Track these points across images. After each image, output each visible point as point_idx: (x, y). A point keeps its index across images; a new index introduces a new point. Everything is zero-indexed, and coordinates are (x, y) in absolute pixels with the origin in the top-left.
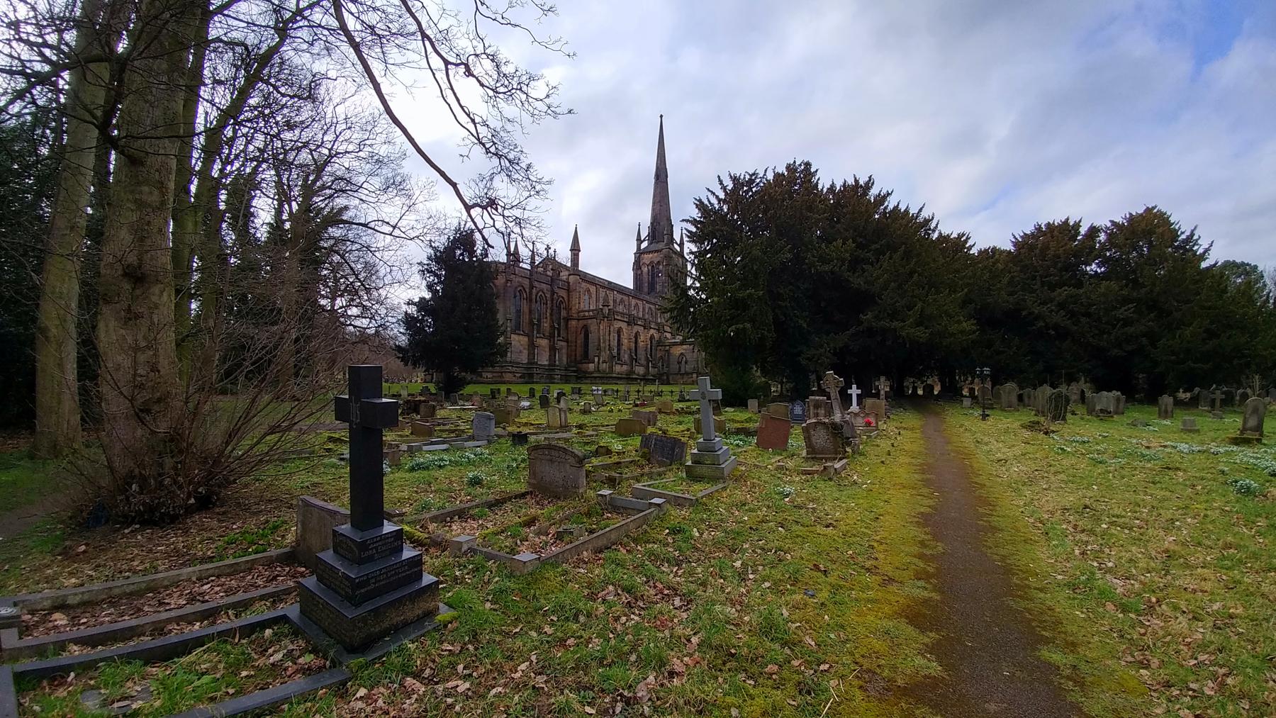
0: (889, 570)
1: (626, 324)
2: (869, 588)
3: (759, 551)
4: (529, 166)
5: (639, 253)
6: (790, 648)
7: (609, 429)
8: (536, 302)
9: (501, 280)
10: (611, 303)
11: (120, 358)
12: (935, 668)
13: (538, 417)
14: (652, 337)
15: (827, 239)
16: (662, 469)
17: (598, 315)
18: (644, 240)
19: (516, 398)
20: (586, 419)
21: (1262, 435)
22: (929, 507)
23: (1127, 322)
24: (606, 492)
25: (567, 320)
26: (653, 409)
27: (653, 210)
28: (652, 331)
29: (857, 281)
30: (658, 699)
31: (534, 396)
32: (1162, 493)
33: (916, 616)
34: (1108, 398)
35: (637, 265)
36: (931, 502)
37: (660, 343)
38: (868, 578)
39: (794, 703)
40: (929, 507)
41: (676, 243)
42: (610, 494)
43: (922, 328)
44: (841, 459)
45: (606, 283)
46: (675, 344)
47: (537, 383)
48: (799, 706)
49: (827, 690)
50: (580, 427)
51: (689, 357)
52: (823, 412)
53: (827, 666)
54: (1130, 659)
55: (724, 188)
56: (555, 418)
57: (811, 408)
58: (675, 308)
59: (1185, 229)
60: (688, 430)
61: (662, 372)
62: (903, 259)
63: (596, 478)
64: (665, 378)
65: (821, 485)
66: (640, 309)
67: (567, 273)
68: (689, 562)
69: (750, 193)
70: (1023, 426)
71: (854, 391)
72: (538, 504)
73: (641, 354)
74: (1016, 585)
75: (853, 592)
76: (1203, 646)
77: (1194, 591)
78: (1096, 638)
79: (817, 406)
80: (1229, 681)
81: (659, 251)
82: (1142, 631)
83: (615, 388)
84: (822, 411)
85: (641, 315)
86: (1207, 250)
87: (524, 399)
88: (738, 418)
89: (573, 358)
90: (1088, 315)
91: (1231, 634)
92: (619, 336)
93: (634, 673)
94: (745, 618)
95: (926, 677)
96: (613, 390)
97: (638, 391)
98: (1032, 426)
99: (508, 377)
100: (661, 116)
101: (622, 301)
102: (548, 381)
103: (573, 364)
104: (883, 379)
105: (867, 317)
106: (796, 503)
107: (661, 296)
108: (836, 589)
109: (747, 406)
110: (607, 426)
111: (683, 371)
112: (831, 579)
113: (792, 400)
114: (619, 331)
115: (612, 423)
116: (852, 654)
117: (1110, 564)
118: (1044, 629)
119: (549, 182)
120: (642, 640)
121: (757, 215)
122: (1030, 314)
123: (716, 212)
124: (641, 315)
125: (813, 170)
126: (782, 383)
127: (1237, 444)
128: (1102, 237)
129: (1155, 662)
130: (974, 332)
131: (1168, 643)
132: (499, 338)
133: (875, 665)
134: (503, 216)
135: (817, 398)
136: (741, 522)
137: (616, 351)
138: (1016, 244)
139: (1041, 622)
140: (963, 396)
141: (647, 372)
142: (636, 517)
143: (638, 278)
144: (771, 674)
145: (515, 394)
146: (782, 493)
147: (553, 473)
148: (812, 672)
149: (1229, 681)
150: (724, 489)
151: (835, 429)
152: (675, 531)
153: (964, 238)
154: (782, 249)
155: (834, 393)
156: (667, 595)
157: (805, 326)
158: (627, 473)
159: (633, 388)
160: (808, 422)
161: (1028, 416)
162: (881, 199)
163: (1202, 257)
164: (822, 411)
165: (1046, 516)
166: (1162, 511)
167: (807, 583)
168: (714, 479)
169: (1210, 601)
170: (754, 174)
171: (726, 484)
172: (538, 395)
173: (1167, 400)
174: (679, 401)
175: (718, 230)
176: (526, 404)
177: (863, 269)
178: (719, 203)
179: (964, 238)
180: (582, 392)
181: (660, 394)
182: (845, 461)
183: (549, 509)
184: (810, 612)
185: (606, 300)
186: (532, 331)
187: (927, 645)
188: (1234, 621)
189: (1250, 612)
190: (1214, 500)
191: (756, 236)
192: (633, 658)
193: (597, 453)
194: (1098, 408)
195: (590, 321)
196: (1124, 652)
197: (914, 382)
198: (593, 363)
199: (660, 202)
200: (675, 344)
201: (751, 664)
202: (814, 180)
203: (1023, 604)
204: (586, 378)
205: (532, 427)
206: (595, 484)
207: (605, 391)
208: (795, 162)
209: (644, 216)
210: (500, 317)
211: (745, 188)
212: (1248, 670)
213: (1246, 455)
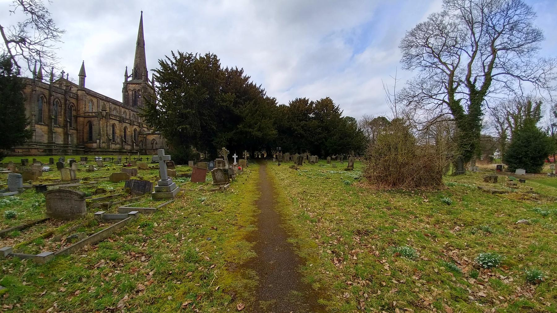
0: (241, 223)
1: (129, 125)
2: (233, 231)
3: (188, 227)
4: (50, 21)
5: (126, 84)
6: (198, 263)
7: (106, 179)
8: (54, 105)
9: (28, 90)
10: (108, 109)
12: (254, 254)
13: (56, 175)
14: (135, 130)
15: (225, 91)
16: (138, 197)
17: (99, 115)
19: (40, 165)
20: (90, 175)
21: (353, 168)
22: (258, 198)
23: (320, 133)
24: (101, 212)
25: (76, 117)
26: (136, 167)
27: (135, 61)
28: (135, 127)
29: (237, 111)
30: (130, 305)
31: (53, 163)
32: (325, 185)
33: (249, 238)
34: (314, 158)
35: (125, 90)
36: (259, 196)
37: (140, 133)
38: (234, 228)
39: (199, 285)
40: (258, 198)
41: (150, 81)
42: (103, 213)
43: (260, 132)
44: (227, 184)
46: (149, 134)
47: (55, 155)
48: (200, 285)
49: (213, 275)
50: (86, 179)
51: (158, 140)
52: (222, 165)
53: (214, 265)
54: (313, 237)
55: (175, 58)
56: (66, 174)
57: (217, 163)
58: (148, 115)
59: (336, 105)
60: (156, 177)
61: (142, 148)
62: (253, 104)
63: (94, 206)
65: (219, 195)
66: (128, 114)
67: (76, 89)
68: (151, 239)
69: (189, 63)
70: (290, 167)
71: (235, 156)
72: (54, 225)
74: (282, 220)
75: (227, 234)
76: (333, 230)
77: (331, 214)
78: (304, 232)
79: (219, 163)
80: (341, 239)
81: (140, 84)
82: (317, 227)
83: (111, 157)
84: (221, 165)
85: (128, 117)
86: (341, 113)
87: (45, 165)
88: (183, 170)
90: (309, 131)
91: (341, 225)
92: (113, 128)
93: (116, 297)
94: (178, 257)
95: (250, 259)
96: (110, 158)
97: (127, 159)
98: (292, 167)
99: (34, 152)
100: (142, 12)
101: (115, 109)
102: (63, 154)
103: (81, 144)
104: (246, 151)
105: (240, 126)
106: (207, 204)
107: (140, 109)
108: (220, 234)
109: (188, 164)
110: (104, 178)
112: (219, 231)
113: (209, 161)
114: (113, 126)
115: (108, 176)
116: (224, 258)
117: (309, 209)
118: (289, 232)
119: (62, 32)
120: (121, 281)
121: (192, 75)
122: (294, 129)
123: (170, 69)
124: (128, 117)
125: (218, 59)
126: (205, 153)
127: (346, 171)
128: (314, 105)
129: (320, 236)
130: (277, 134)
131: (323, 230)
132: (26, 127)
133: (233, 260)
134: (29, 48)
135: (219, 159)
136: (180, 216)
137: (111, 136)
138: (290, 104)
139: (288, 230)
140: (273, 158)
142: (119, 223)
143: (125, 97)
144: (189, 276)
145: (39, 162)
146: (201, 200)
147: (62, 206)
148: (207, 270)
149: (341, 239)
150: (173, 202)
151: (225, 172)
152: (143, 226)
153: (274, 100)
154: (204, 93)
155: (226, 157)
156: (138, 257)
157: (215, 128)
158: (116, 201)
159: (123, 157)
160: (214, 169)
161: (292, 164)
162: (246, 79)
163: (340, 115)
164: (221, 165)
165: (293, 196)
166: (324, 191)
167: (208, 235)
168: (167, 198)
169: (335, 216)
170: (191, 54)
171: (174, 200)
172: (55, 162)
173: (329, 158)
174: (152, 163)
175: (172, 78)
176: (47, 168)
177: (239, 106)
178: (172, 64)
179: (274, 100)
180: (88, 160)
181: (140, 160)
182: (229, 184)
183: (62, 226)
184: (208, 246)
185: (104, 107)
186: (51, 122)
187: (252, 247)
188: (342, 221)
189: (347, 218)
190: (338, 187)
191: (192, 84)
192: (116, 290)
193: (96, 193)
194: (311, 161)
195: (93, 119)
196: (311, 235)
197: (258, 153)
198: (96, 143)
199: (140, 57)
200: (149, 134)
201: (180, 276)
202: (218, 63)
203: (284, 225)
204: (91, 152)
205: (50, 181)
206: (94, 210)
207: (104, 159)
208: (209, 53)
209: (130, 63)
210: (27, 114)
211: (186, 60)
212: (347, 236)
213: (348, 173)
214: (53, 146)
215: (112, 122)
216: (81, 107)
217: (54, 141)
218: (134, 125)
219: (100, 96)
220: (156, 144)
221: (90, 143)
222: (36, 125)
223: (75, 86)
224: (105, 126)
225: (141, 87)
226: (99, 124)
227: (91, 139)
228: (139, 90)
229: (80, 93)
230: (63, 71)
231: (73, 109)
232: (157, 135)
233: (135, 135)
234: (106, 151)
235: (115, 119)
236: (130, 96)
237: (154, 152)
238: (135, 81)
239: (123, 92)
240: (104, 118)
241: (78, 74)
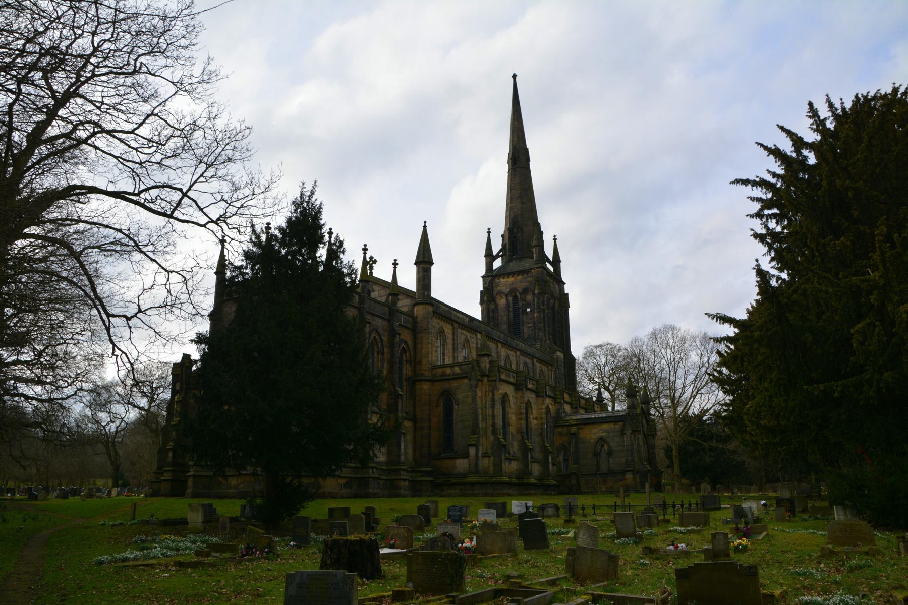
5: (490, 277)
11: (666, 401)
18: (498, 256)
25: (413, 382)
45: (467, 319)
64: (574, 482)
73: (534, 442)
100: (514, 76)
111: (604, 468)
141: (525, 472)
195: (455, 384)
198: (466, 456)
216: (424, 351)
219: (458, 317)
220: (610, 453)
221: (449, 458)
223: (406, 293)
224: (489, 405)
226: (474, 398)
227: (449, 447)
228: (525, 291)
231: (404, 359)
232: (612, 425)
234: (493, 484)
235: (507, 379)
238: (514, 266)
239: (482, 302)
240: (486, 379)
241: (414, 262)
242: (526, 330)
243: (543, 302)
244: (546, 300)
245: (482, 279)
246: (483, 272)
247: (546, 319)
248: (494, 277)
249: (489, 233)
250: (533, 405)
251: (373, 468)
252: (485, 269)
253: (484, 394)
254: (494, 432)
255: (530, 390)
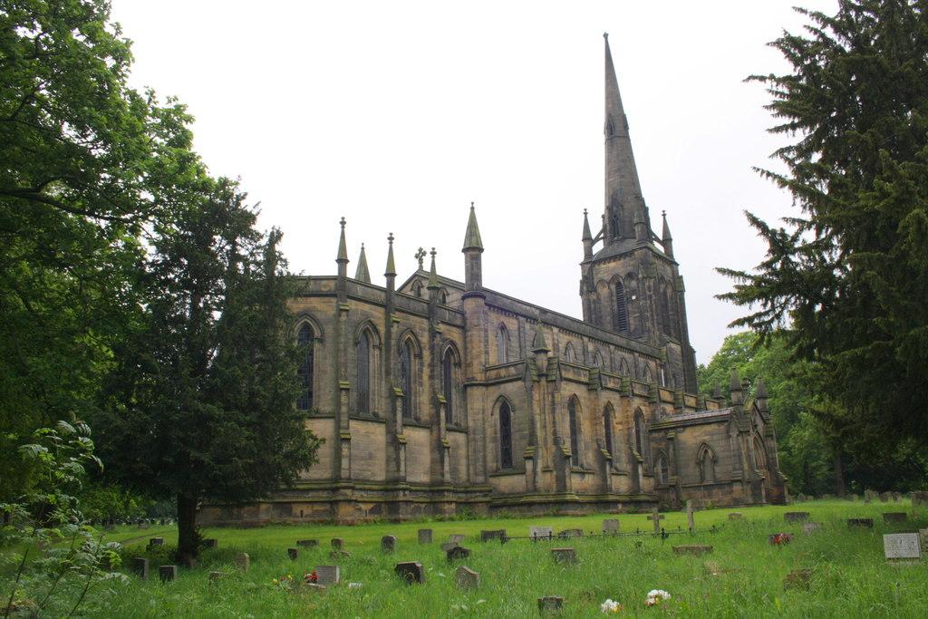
1: (583, 388)
5: (590, 263)
14: (638, 414)
18: (598, 239)
28: (637, 402)
35: (588, 286)
41: (657, 240)
51: (719, 447)
89: (480, 464)
100: (606, 36)
114: (573, 402)
143: (588, 308)
185: (538, 339)
214: (399, 489)
215: (567, 390)
217: (402, 474)
218: (634, 395)
220: (715, 461)
222: (353, 424)
223: (455, 285)
225: (632, 263)
228: (630, 276)
229: (470, 305)
230: (420, 250)
231: (452, 362)
233: (638, 432)
235: (576, 378)
236: (603, 302)
237: (710, 496)
239: (582, 293)
240: (543, 381)
242: (632, 321)
243: (649, 287)
244: (652, 284)
245: (580, 267)
246: (581, 258)
247: (654, 307)
248: (595, 262)
249: (586, 214)
250: (615, 407)
251: (404, 490)
252: (583, 256)
253: (542, 397)
254: (556, 441)
255: (637, 395)
